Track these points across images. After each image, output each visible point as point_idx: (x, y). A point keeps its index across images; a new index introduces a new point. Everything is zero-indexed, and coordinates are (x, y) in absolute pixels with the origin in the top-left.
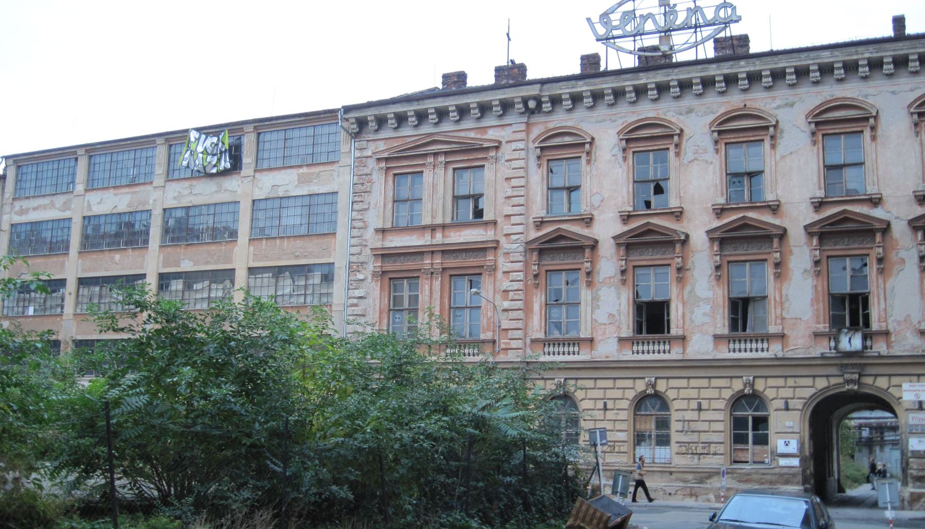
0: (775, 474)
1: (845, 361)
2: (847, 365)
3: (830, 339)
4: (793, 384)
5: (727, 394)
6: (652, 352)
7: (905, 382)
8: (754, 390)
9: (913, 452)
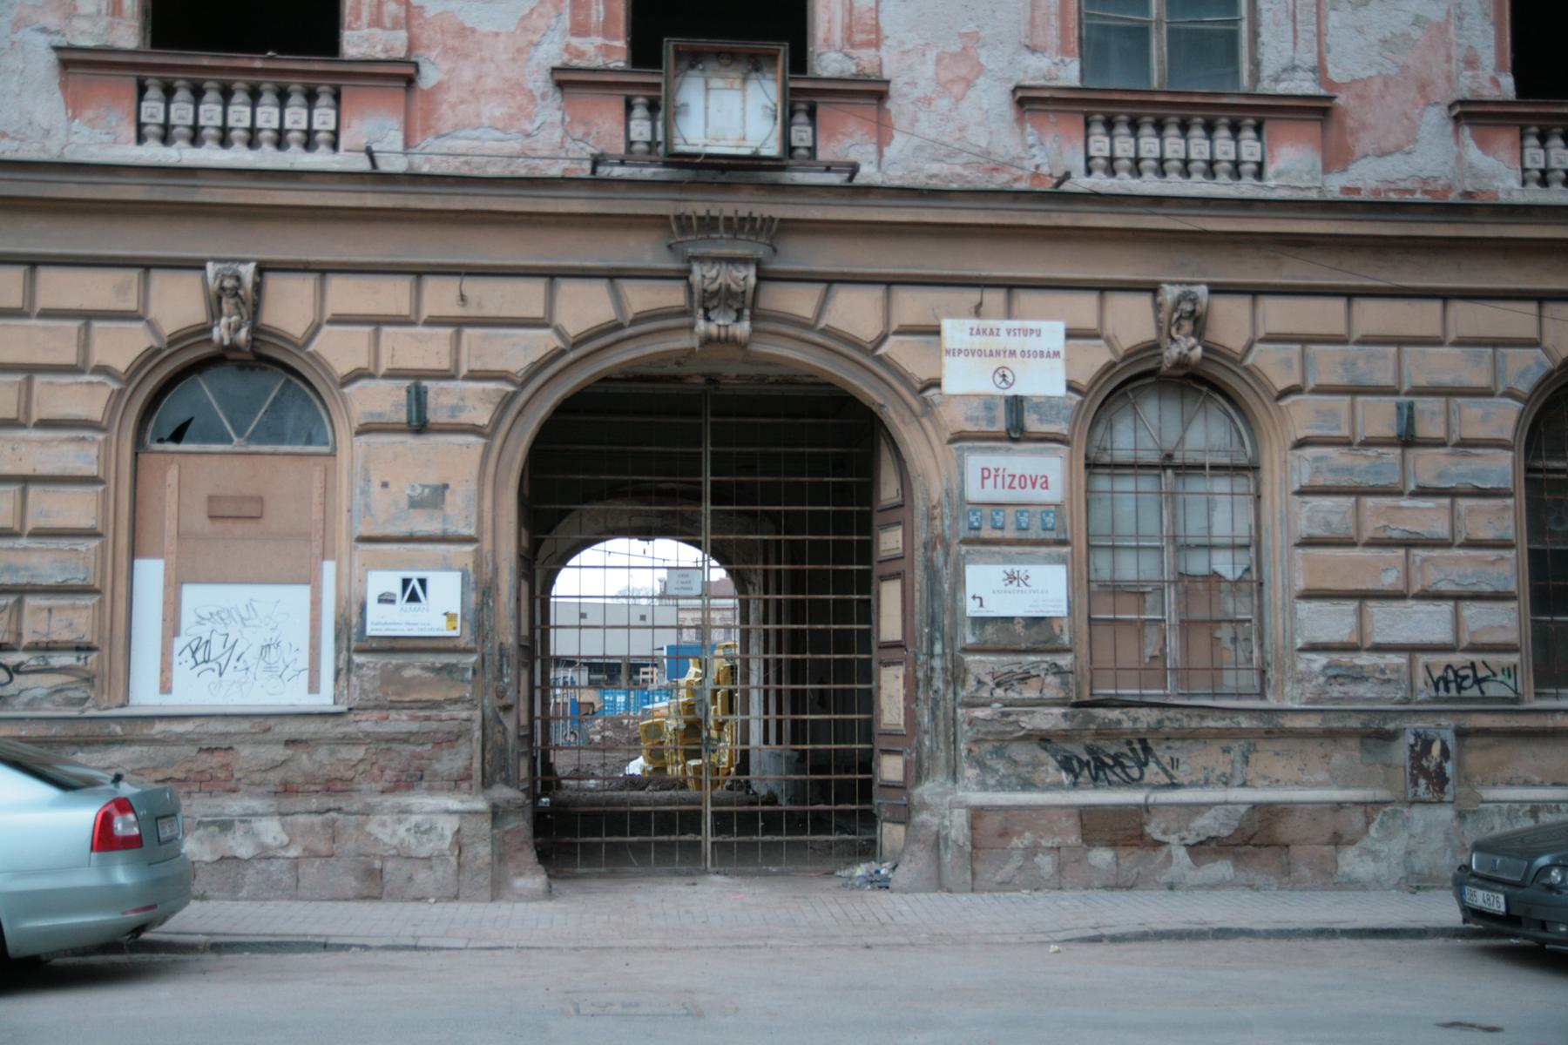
0: (349, 740)
1: (698, 206)
2: (708, 224)
3: (629, 107)
4: (455, 310)
5: (121, 347)
6: (243, 131)
7: (952, 315)
8: (257, 331)
9: (981, 622)
